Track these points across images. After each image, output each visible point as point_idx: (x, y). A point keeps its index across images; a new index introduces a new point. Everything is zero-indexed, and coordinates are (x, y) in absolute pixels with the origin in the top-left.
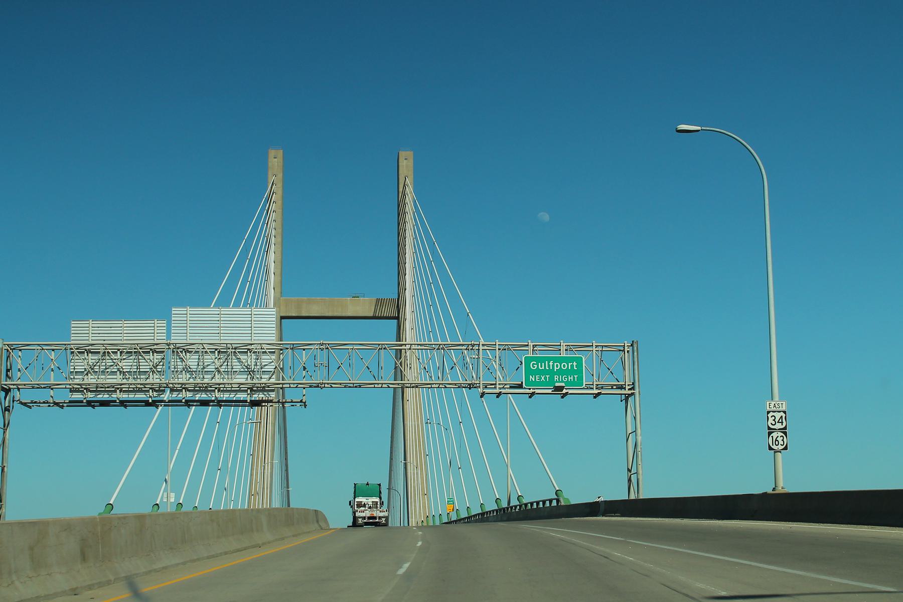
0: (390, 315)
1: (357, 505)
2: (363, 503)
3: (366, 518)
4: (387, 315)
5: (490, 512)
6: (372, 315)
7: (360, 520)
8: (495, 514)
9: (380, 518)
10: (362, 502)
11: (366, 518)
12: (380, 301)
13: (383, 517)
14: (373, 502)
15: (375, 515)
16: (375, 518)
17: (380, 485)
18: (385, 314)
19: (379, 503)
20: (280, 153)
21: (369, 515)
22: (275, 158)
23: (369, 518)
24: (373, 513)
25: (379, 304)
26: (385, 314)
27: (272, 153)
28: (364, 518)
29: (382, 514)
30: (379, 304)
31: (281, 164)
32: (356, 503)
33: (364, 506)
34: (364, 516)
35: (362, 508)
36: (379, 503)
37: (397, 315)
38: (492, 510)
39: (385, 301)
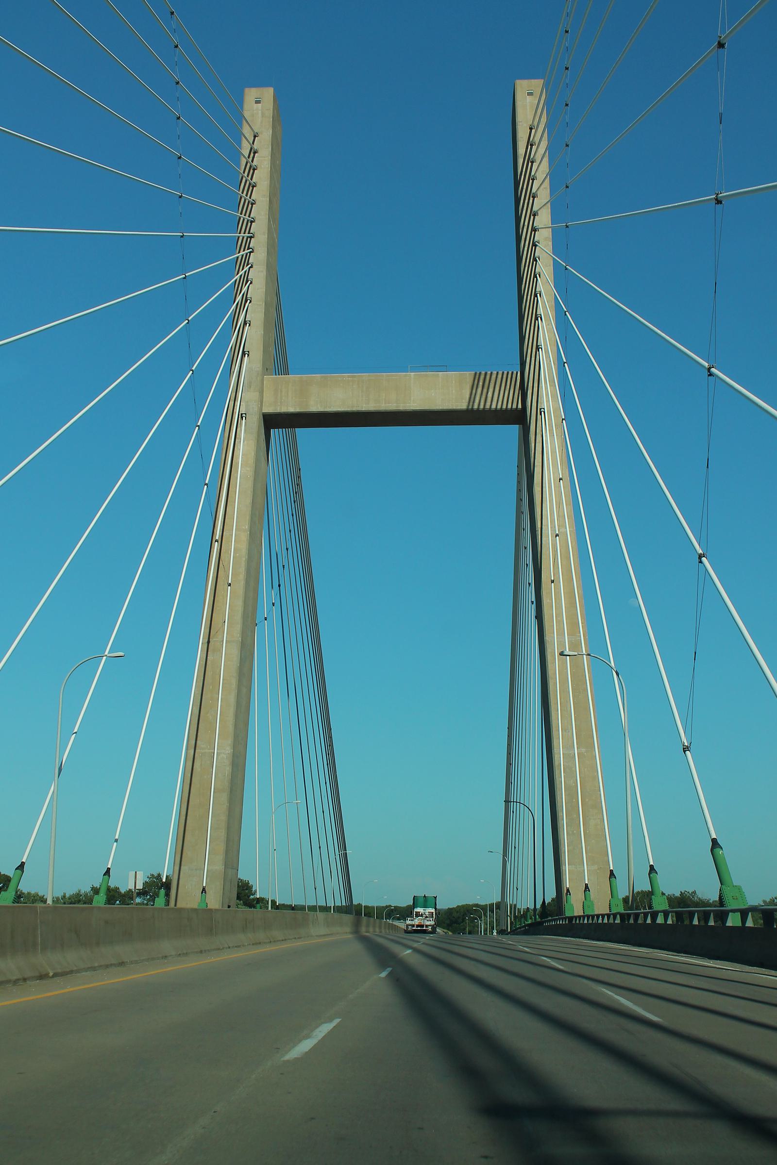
0: (504, 407)
1: (415, 914)
2: (421, 913)
3: (415, 926)
4: (499, 407)
5: (598, 916)
6: (463, 406)
7: (410, 927)
8: (618, 921)
9: (427, 926)
10: (419, 912)
11: (415, 926)
12: (482, 377)
13: (429, 926)
14: (429, 912)
15: (422, 924)
16: (422, 926)
17: (435, 898)
18: (500, 403)
19: (434, 914)
20: (268, 93)
21: (417, 923)
22: (257, 102)
23: (418, 926)
24: (421, 921)
25: (481, 383)
26: (500, 403)
27: (251, 94)
28: (413, 926)
29: (428, 923)
30: (481, 383)
31: (269, 113)
32: (415, 913)
33: (422, 916)
34: (414, 924)
35: (419, 917)
36: (434, 914)
37: (520, 406)
38: (592, 916)
39: (494, 376)
